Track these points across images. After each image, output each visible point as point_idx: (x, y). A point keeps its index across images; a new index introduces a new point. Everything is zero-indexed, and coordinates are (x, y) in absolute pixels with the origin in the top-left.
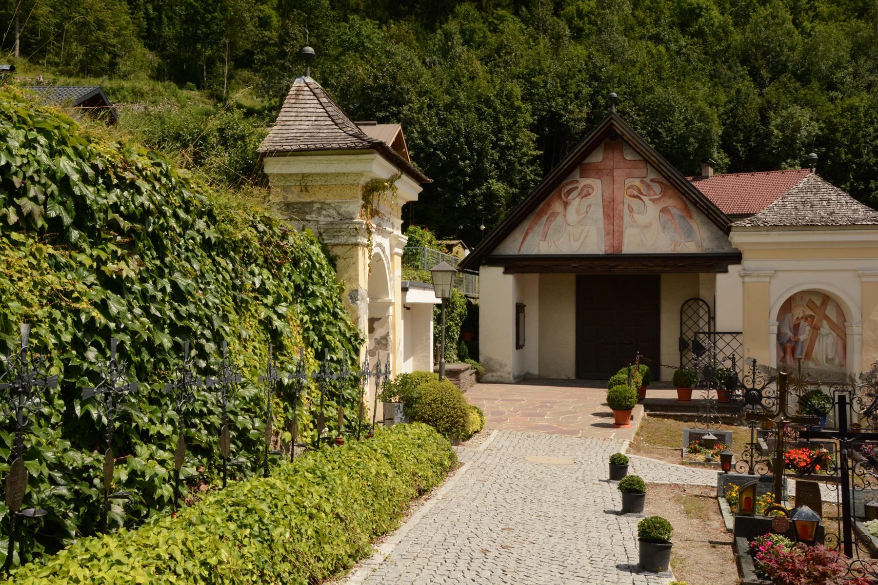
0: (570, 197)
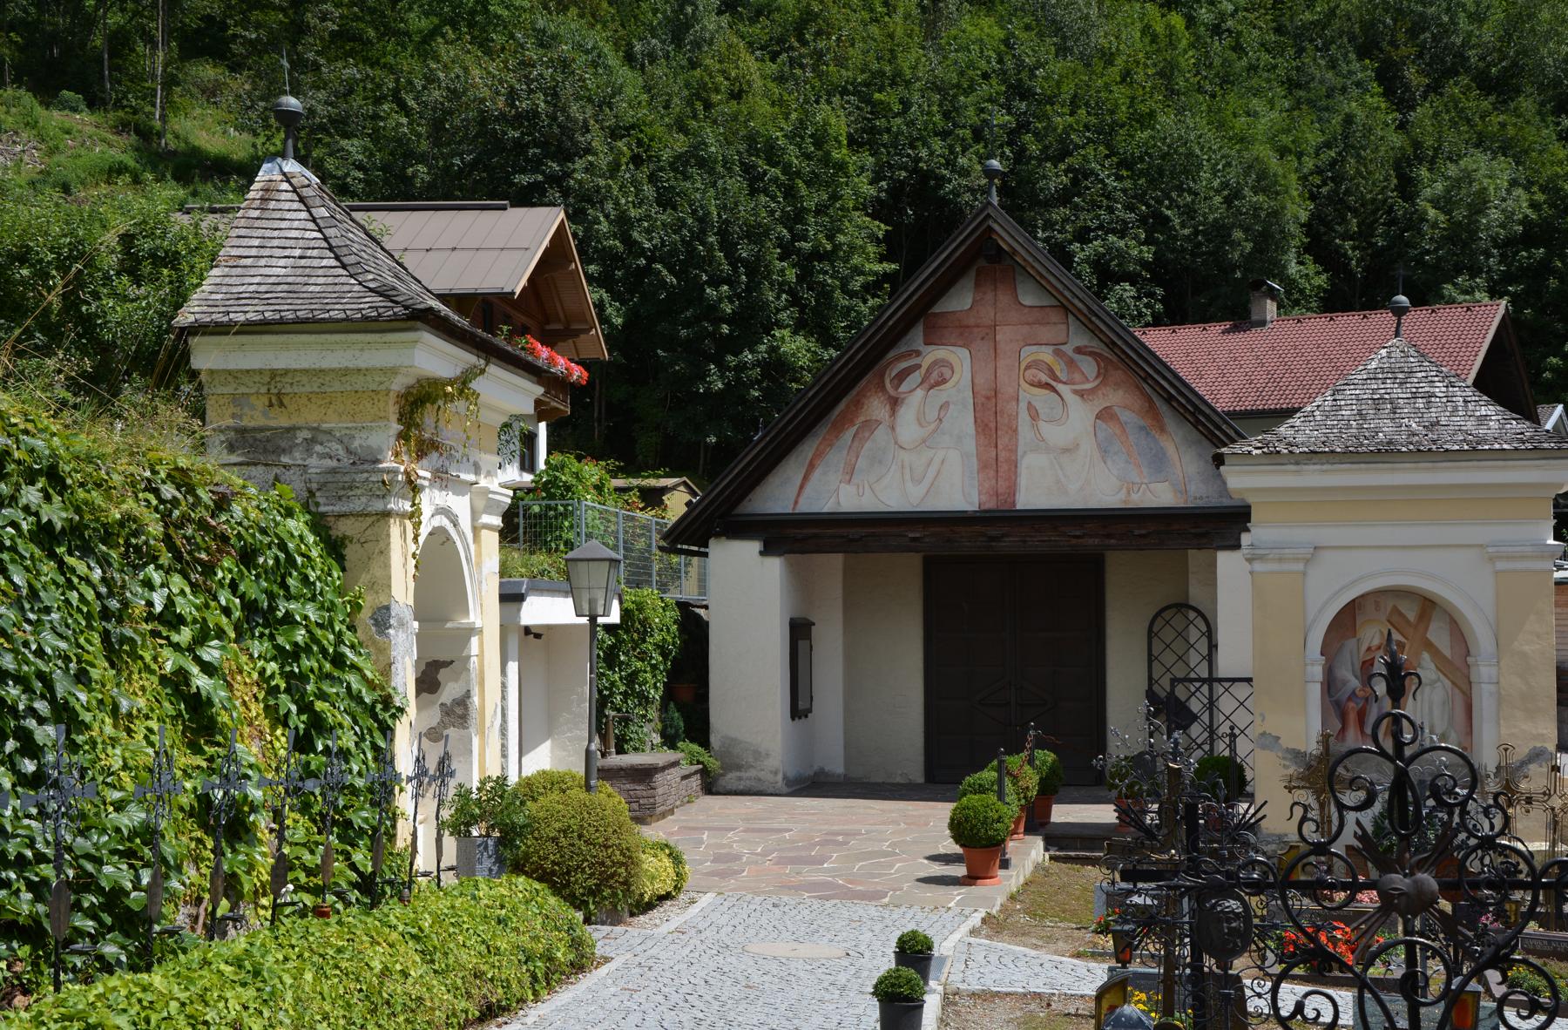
0: (904, 388)
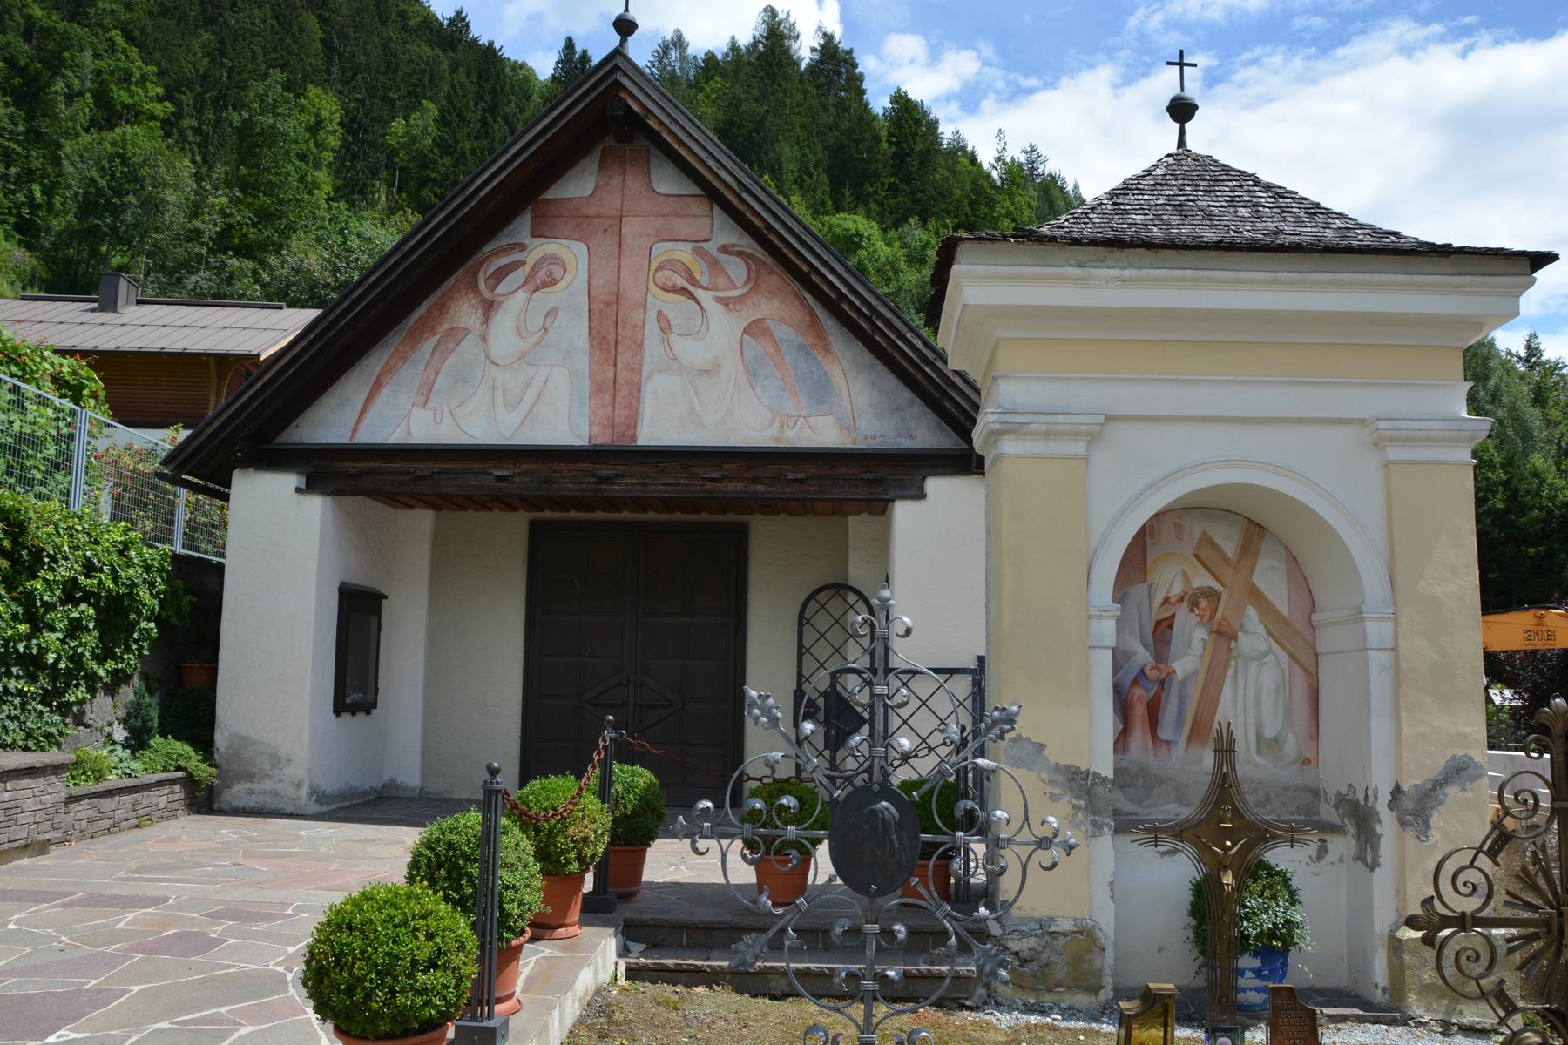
0: (500, 289)
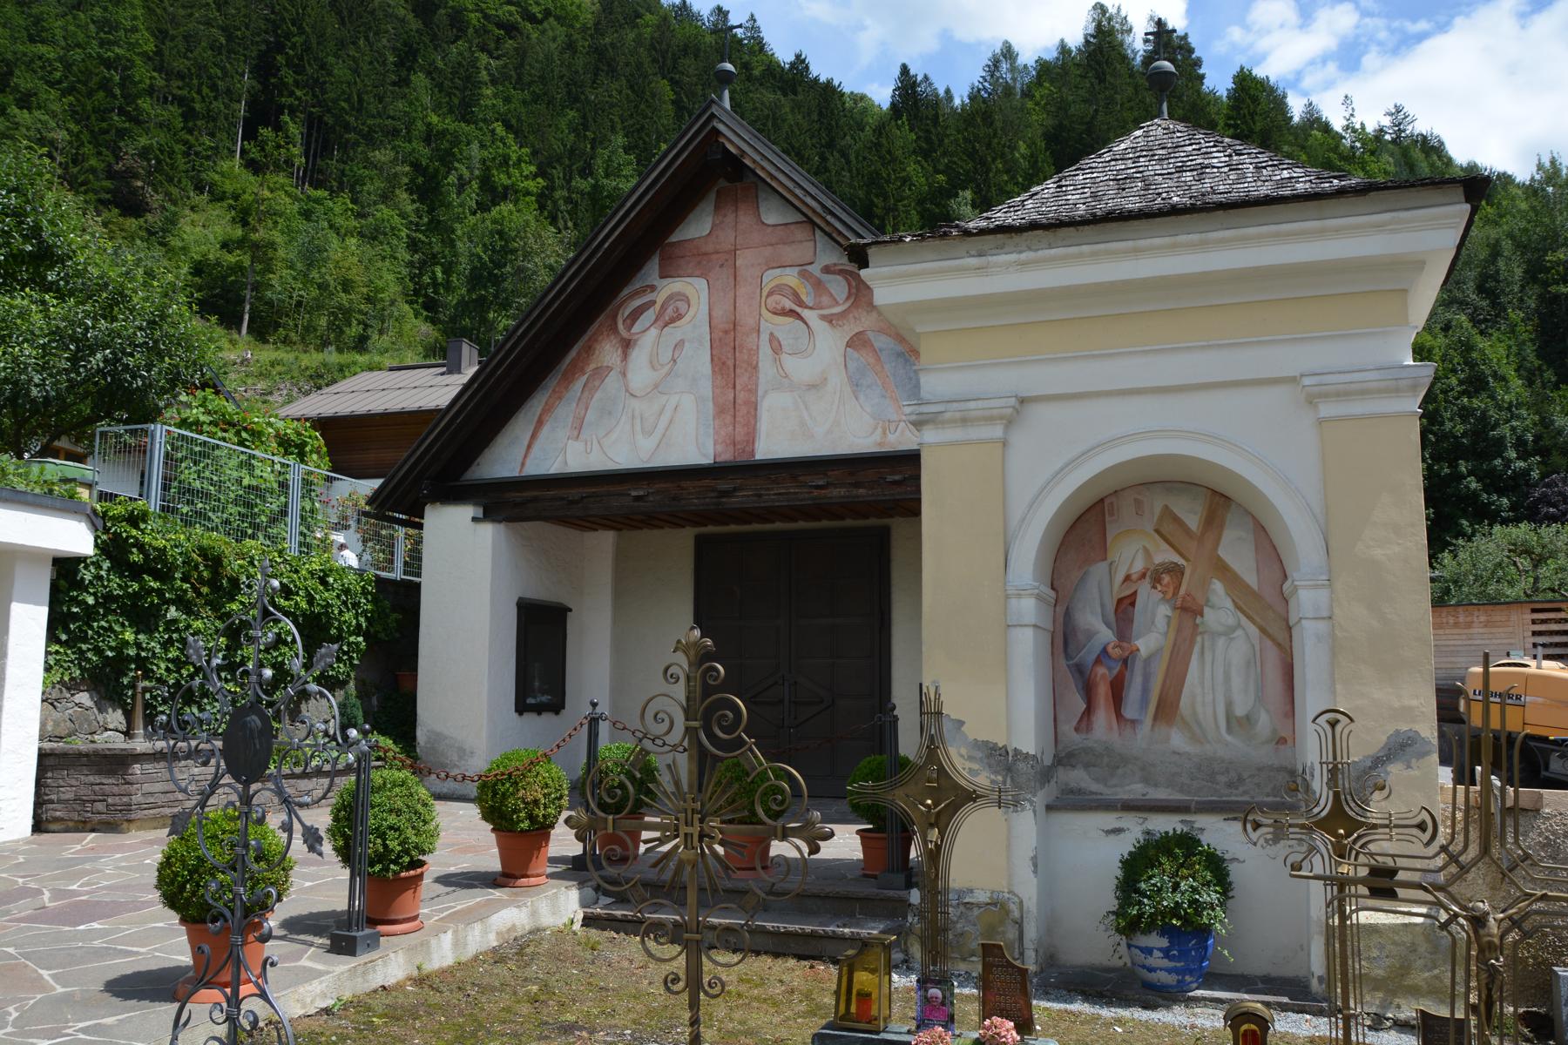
0: (636, 328)
